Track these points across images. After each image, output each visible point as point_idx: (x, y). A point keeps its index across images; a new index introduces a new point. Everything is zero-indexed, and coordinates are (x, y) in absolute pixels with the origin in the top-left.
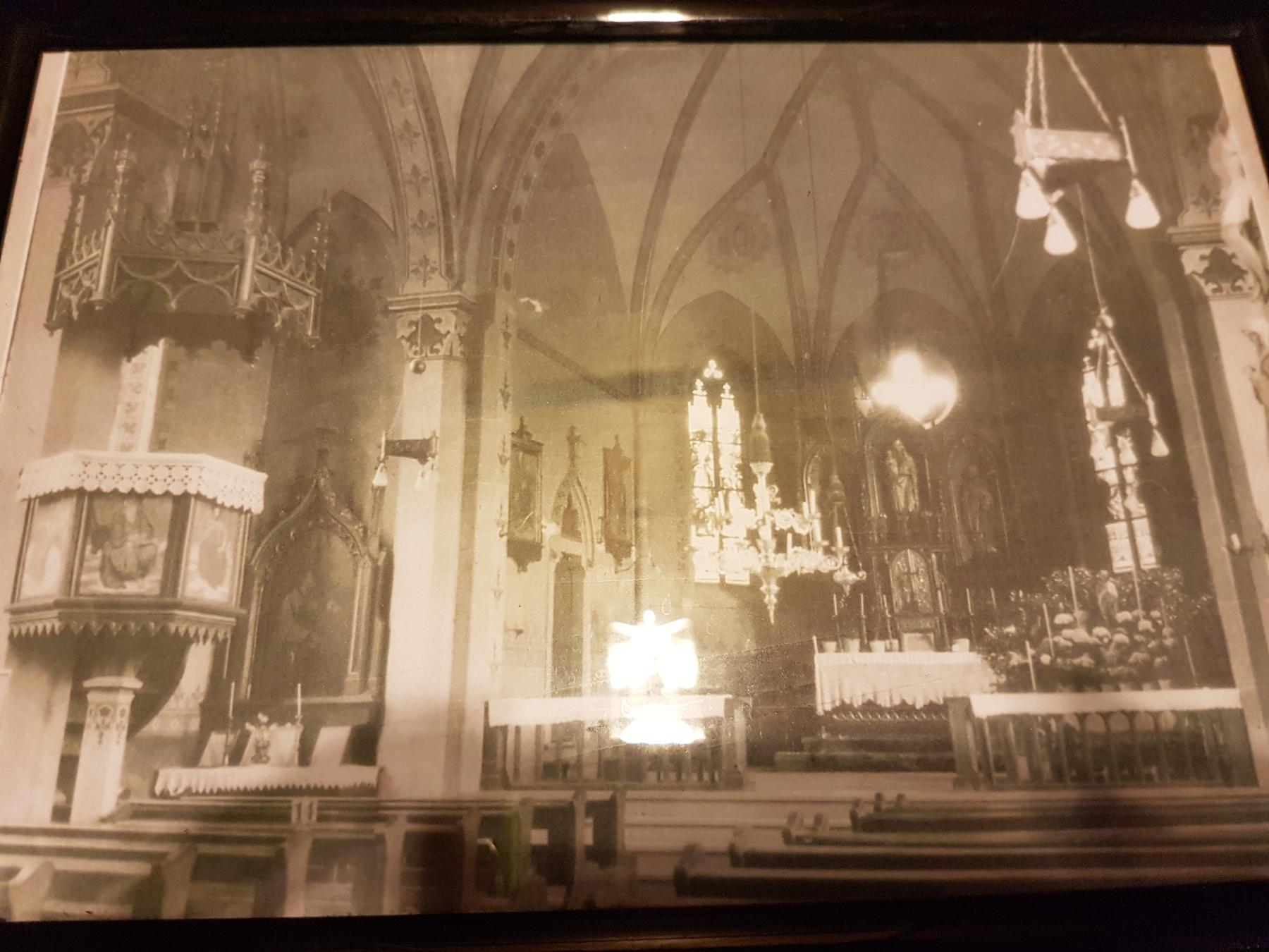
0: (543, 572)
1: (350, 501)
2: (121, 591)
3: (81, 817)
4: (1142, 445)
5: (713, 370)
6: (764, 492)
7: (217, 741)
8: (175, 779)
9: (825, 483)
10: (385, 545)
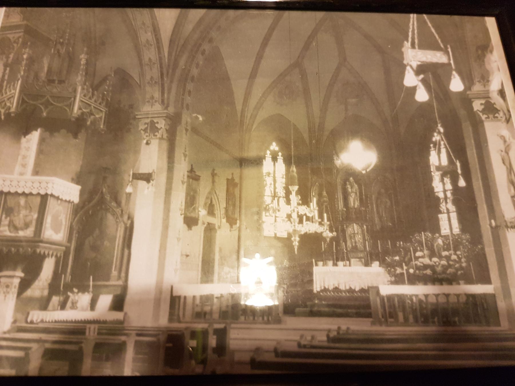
0: (199, 230)
5: (274, 147)
6: (294, 198)
7: (55, 300)
9: (320, 195)
10: (131, 218)
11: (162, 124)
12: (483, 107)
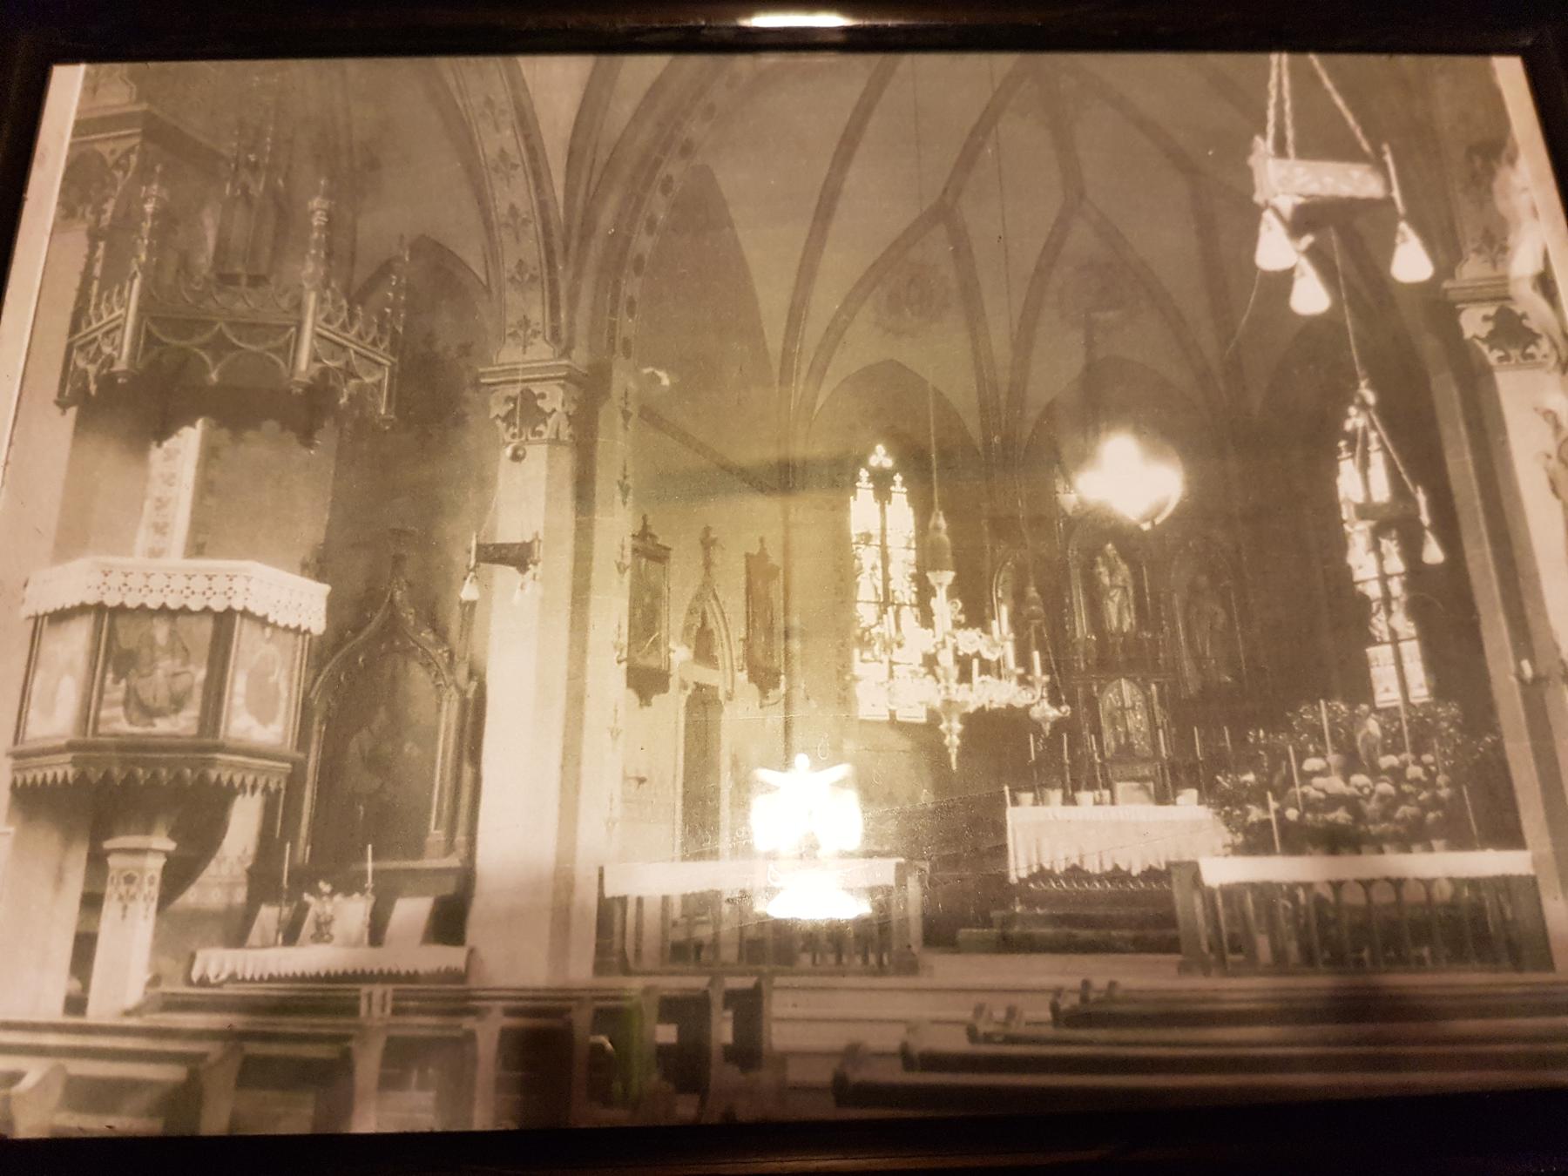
0: (671, 706)
1: (433, 619)
2: (149, 729)
3: (100, 1009)
4: (1411, 550)
5: (881, 457)
6: (944, 608)
7: (269, 915)
8: (216, 962)
9: (1019, 597)
10: (476, 673)
11: (555, 400)
12: (1489, 326)
